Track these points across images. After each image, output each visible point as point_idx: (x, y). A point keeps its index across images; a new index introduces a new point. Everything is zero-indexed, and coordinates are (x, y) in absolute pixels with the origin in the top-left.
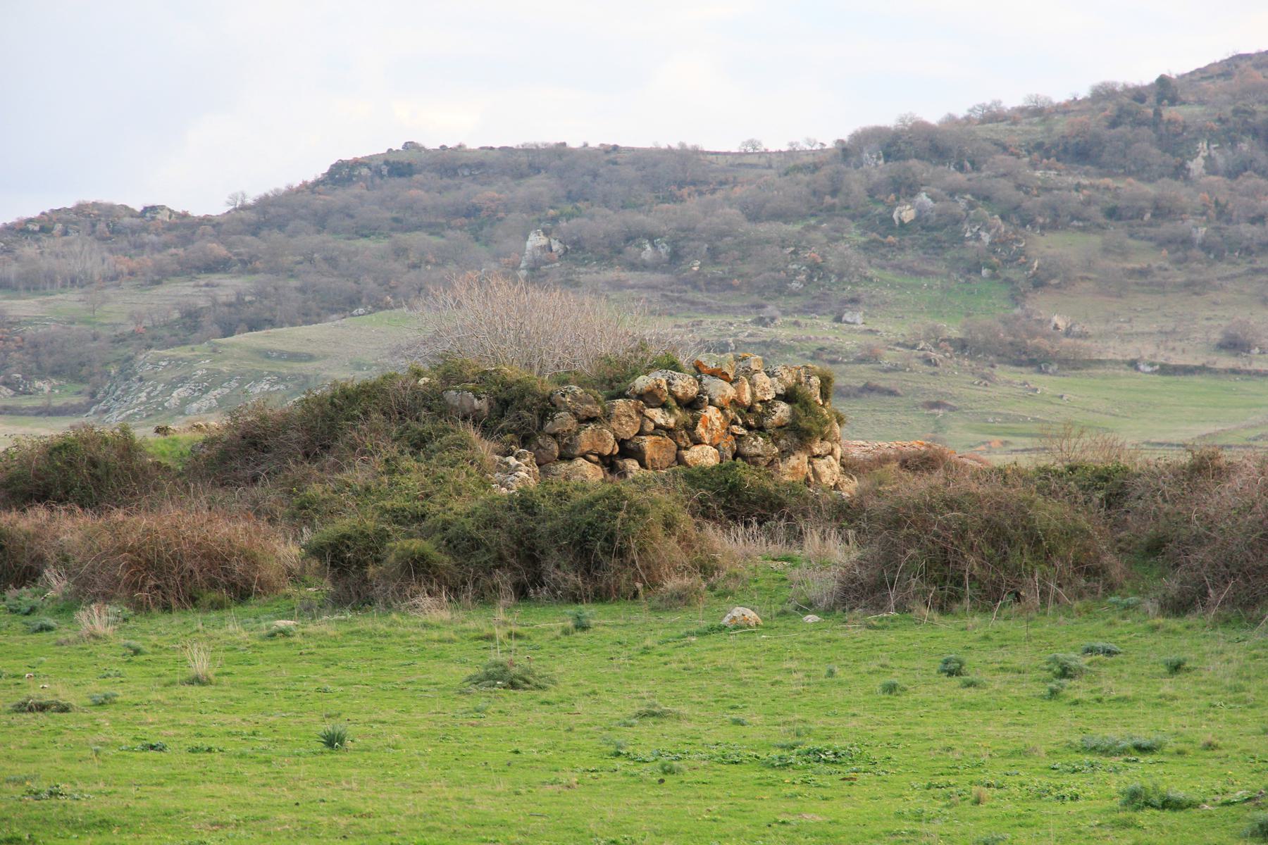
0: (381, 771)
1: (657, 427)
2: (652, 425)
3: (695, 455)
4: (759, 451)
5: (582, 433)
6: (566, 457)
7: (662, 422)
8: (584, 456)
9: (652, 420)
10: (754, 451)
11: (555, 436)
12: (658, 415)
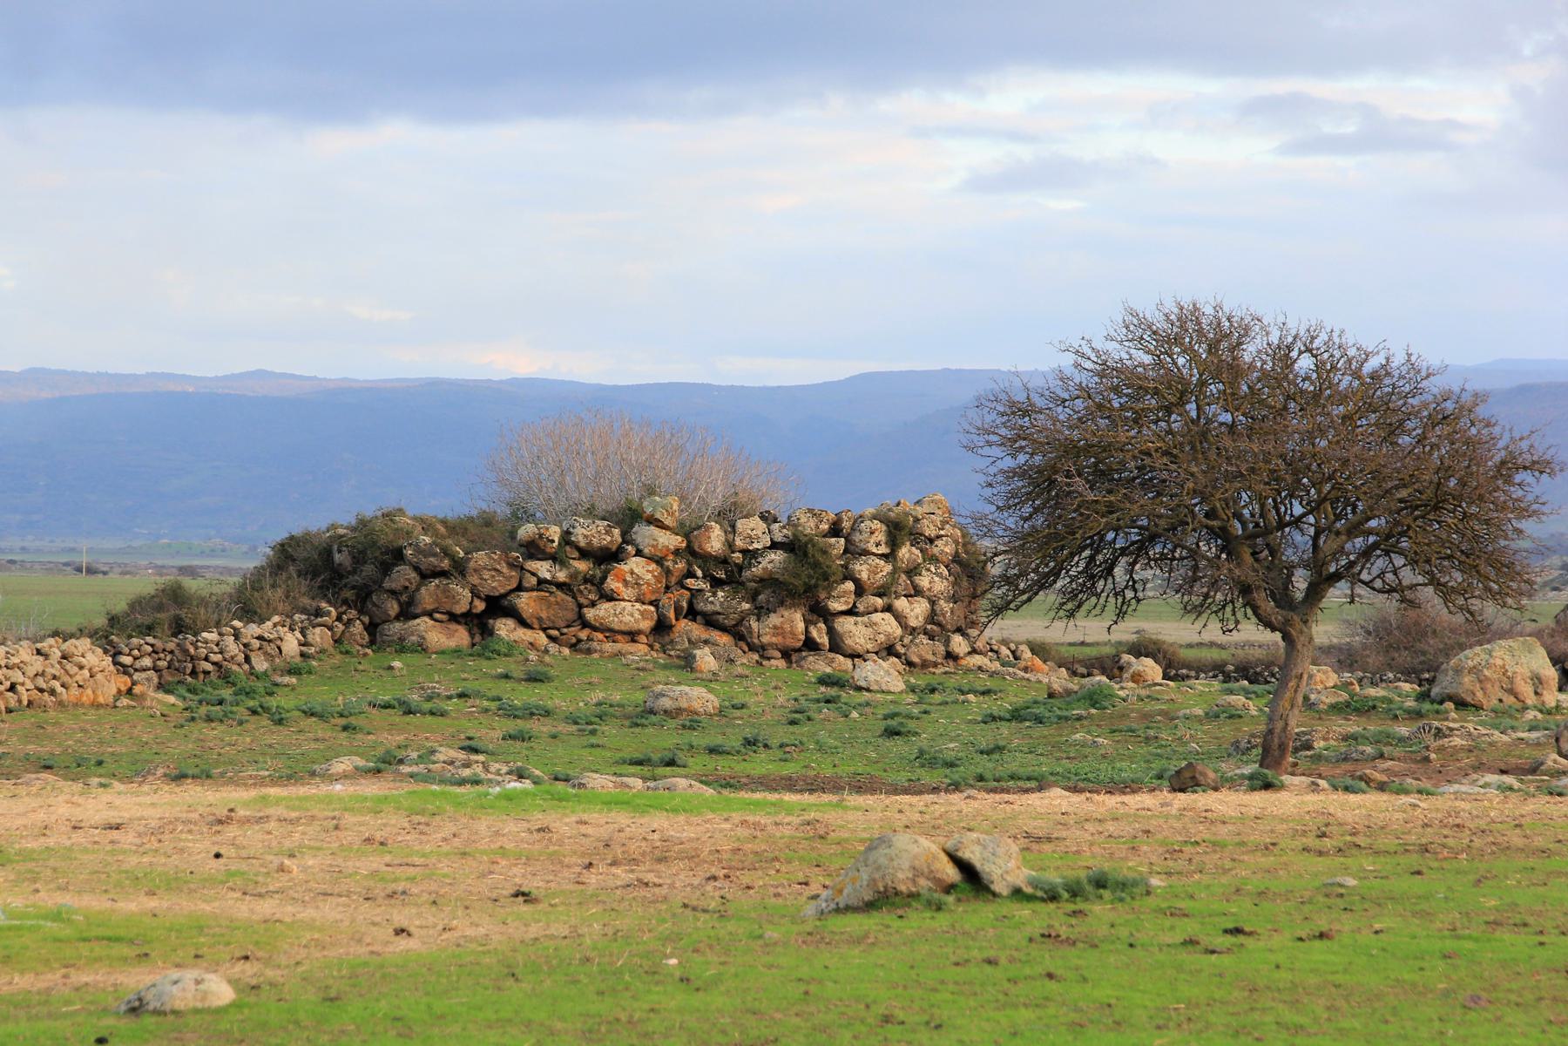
0: (803, 987)
1: (541, 581)
2: (534, 581)
3: (602, 613)
4: (718, 608)
5: (423, 590)
6: (407, 614)
7: (548, 576)
8: (430, 614)
9: (534, 574)
10: (710, 608)
11: (393, 593)
12: (544, 569)
